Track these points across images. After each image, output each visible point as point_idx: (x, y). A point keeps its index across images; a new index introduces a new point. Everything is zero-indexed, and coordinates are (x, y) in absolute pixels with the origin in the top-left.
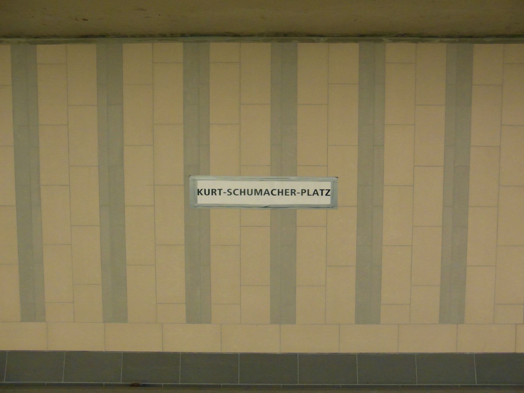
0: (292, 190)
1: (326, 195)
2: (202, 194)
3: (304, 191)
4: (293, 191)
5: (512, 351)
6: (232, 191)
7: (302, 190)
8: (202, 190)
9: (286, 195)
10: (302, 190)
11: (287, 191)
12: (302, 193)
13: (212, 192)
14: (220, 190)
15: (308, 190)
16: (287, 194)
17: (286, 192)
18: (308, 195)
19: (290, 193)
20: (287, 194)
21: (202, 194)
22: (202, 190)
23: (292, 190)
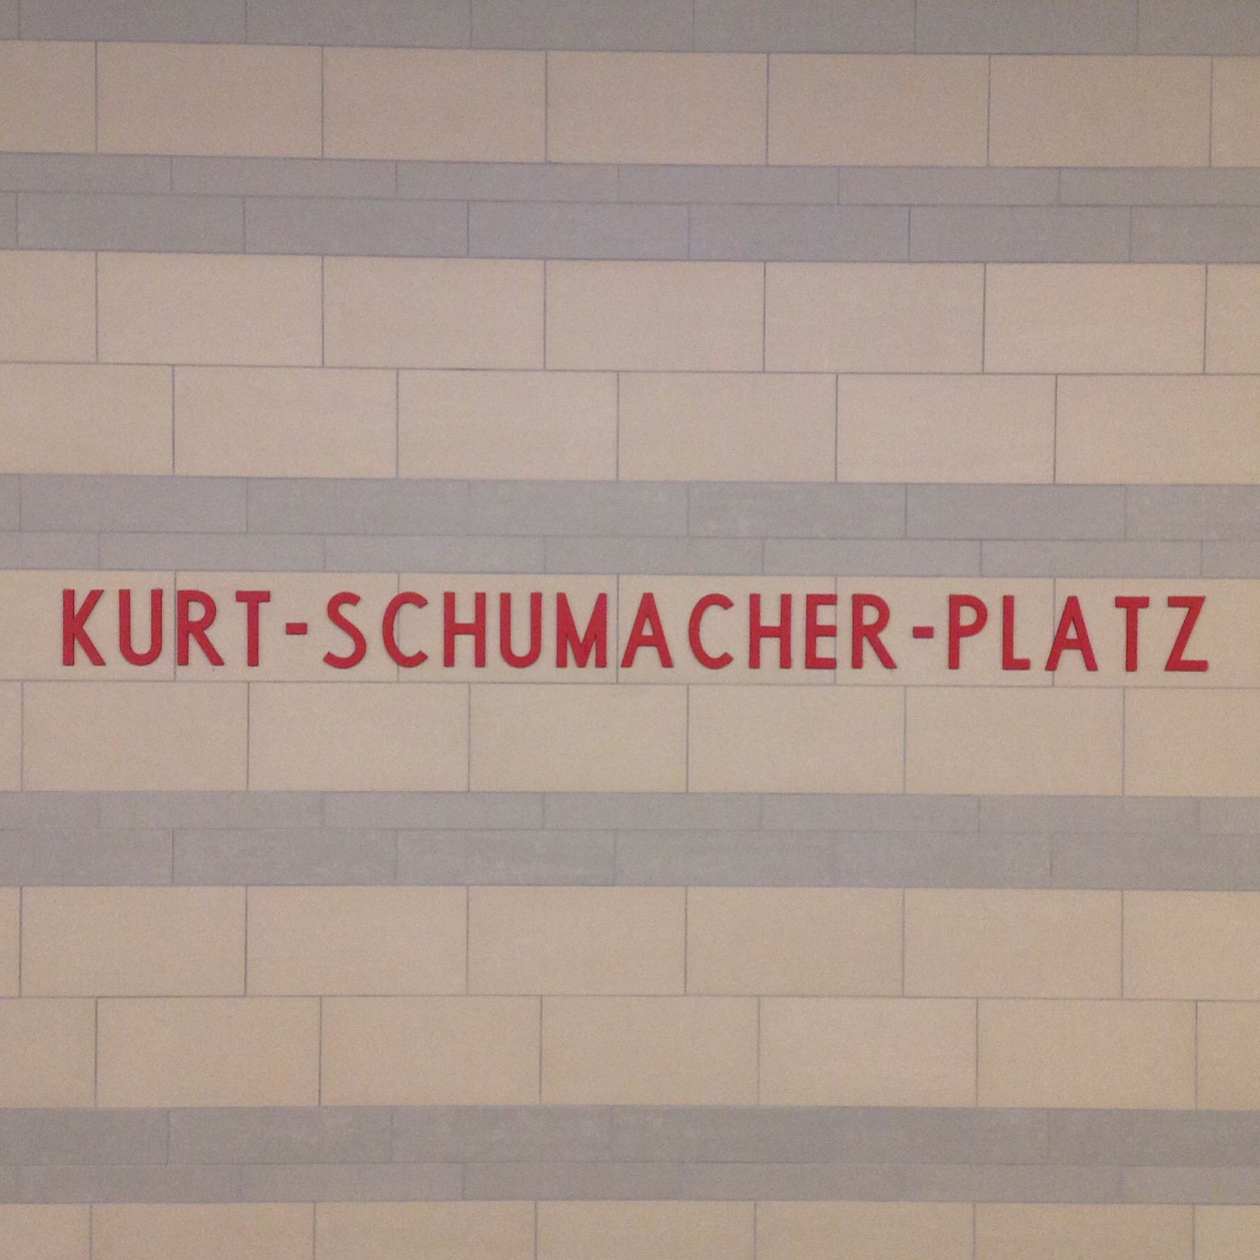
0: (859, 601)
1: (1175, 663)
2: (215, 659)
3: (968, 616)
4: (196, 612)
5: (1001, 274)
6: (367, 618)
7: (956, 602)
8: (95, 596)
9: (813, 662)
10: (956, 602)
11: (825, 616)
12: (957, 632)
13: (186, 629)
14: (253, 600)
15: (1008, 603)
16: (825, 647)
17: (815, 631)
18: (1011, 662)
19: (836, 647)
20: (825, 647)
21: (215, 659)
22: (95, 596)
23: (859, 601)
